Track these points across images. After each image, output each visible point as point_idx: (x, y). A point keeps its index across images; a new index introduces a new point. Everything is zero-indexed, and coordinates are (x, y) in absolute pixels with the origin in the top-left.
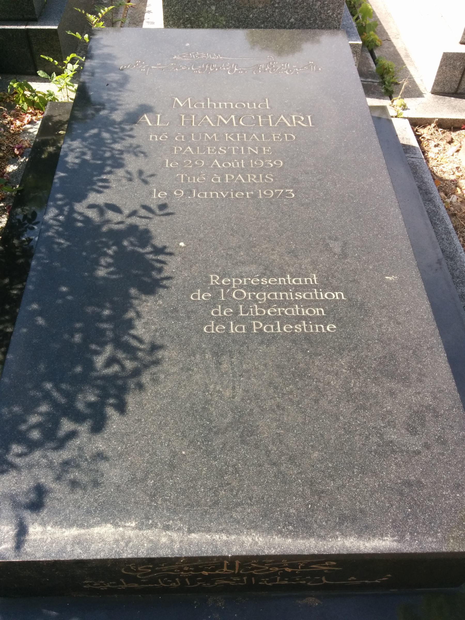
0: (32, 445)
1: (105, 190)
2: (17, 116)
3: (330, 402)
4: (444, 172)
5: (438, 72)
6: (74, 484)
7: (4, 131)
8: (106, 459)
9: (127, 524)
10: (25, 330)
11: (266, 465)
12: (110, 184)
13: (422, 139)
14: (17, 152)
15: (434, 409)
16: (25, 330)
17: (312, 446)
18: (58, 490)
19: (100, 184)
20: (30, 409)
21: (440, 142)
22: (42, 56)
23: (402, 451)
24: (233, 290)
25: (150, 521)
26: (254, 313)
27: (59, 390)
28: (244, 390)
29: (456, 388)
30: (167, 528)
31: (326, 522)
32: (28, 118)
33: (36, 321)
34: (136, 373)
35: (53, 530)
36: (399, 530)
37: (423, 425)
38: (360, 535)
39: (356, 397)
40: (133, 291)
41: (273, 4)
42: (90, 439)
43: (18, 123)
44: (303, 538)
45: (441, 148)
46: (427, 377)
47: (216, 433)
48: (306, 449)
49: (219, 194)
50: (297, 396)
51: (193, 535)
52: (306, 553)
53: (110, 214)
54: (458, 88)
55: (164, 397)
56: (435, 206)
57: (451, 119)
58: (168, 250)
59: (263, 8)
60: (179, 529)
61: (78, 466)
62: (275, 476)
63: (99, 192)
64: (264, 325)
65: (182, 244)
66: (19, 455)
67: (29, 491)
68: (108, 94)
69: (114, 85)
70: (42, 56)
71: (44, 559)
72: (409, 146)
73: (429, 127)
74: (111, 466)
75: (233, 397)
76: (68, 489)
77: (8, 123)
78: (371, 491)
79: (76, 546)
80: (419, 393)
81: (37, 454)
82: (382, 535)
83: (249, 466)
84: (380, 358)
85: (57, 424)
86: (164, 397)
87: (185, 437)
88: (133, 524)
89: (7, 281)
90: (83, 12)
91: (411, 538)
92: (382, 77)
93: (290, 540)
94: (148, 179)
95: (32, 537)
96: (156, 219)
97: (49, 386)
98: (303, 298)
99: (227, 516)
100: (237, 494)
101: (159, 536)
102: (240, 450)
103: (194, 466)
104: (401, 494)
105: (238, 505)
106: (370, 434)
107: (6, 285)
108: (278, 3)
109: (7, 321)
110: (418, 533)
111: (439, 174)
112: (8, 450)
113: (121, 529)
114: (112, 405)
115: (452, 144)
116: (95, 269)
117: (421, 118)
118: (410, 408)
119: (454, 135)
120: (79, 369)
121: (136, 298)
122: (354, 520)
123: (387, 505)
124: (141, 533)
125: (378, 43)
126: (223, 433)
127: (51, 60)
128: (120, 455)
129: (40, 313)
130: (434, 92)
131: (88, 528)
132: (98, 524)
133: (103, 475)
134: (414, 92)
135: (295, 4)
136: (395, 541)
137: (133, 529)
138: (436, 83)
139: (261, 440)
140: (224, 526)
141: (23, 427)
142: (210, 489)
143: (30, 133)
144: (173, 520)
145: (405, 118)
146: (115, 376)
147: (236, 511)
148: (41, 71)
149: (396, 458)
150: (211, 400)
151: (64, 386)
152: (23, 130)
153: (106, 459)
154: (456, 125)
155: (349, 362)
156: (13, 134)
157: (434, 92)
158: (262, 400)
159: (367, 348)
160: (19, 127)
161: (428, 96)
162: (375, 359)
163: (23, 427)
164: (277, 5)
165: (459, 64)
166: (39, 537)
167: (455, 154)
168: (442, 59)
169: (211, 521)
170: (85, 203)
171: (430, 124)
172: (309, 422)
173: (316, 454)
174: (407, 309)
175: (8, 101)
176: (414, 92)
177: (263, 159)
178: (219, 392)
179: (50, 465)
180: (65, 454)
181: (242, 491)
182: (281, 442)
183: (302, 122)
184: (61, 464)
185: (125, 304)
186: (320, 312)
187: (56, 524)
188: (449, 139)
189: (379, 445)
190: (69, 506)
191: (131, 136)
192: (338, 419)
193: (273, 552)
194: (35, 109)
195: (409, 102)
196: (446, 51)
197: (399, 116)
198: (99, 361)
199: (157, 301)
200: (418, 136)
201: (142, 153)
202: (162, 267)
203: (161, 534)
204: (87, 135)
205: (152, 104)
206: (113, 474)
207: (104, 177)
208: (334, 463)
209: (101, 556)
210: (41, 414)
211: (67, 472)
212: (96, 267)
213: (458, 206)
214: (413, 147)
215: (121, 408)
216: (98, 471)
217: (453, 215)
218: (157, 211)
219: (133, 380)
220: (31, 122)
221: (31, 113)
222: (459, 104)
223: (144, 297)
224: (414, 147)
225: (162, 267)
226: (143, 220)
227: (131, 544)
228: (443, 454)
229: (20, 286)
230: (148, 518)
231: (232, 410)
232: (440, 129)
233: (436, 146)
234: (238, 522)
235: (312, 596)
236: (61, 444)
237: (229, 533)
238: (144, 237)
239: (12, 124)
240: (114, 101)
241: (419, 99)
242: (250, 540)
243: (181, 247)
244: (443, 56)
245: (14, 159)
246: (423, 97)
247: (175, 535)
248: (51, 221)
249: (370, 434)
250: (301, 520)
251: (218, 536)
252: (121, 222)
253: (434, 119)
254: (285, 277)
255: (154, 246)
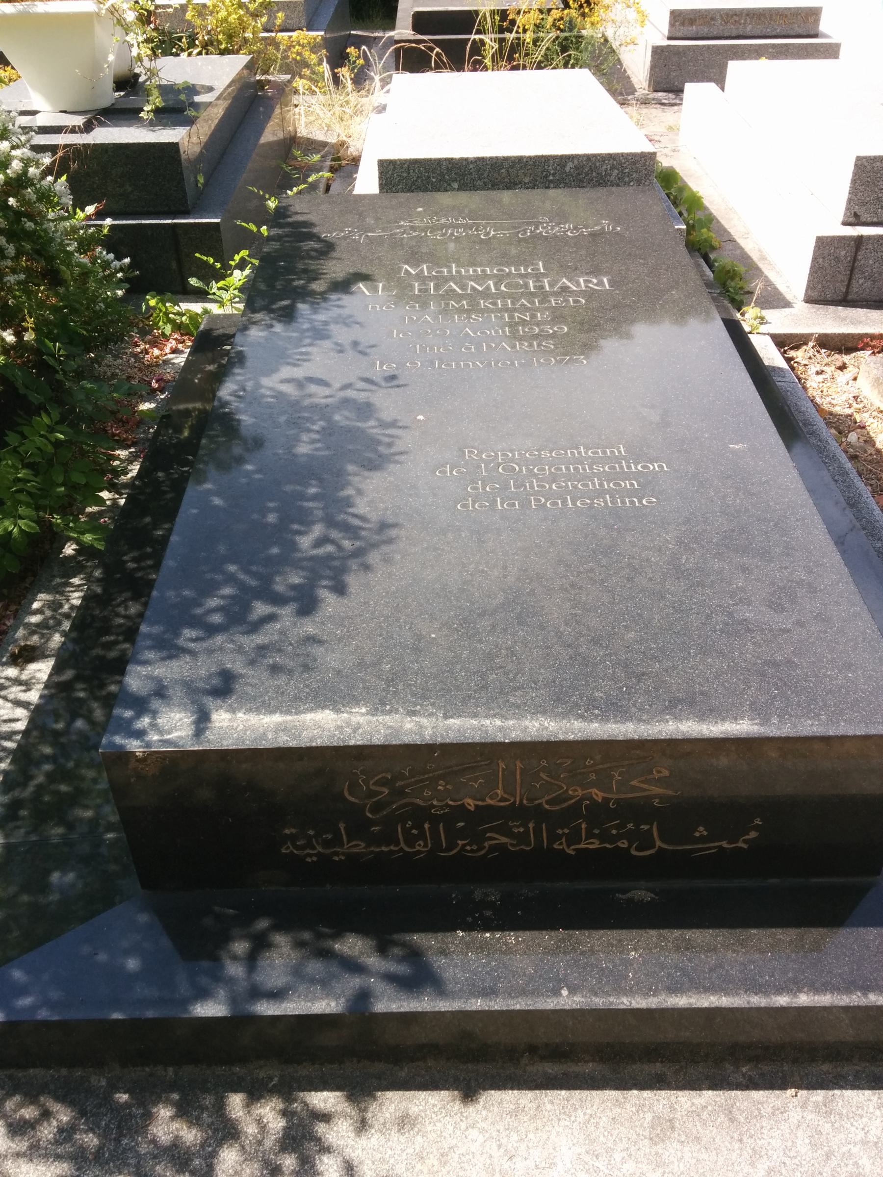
0: (212, 630)
1: (305, 363)
2: (154, 343)
3: (650, 579)
4: (834, 406)
5: (811, 268)
6: (275, 669)
7: (135, 362)
8: (320, 642)
9: (354, 710)
10: (195, 511)
11: (557, 647)
12: (312, 357)
13: (795, 365)
14: (155, 385)
15: (810, 585)
16: (195, 511)
17: (625, 627)
18: (252, 677)
19: (298, 357)
20: (209, 589)
21: (826, 369)
22: (197, 255)
23: (762, 630)
24: (499, 465)
25: (388, 707)
26: (532, 487)
27: (248, 572)
28: (521, 570)
29: (842, 561)
30: (413, 713)
31: (650, 706)
32: (172, 344)
33: (211, 501)
34: (358, 553)
35: (246, 717)
36: (759, 712)
37: (793, 601)
38: (701, 718)
39: (690, 574)
40: (351, 468)
41: (546, 177)
42: (295, 623)
43: (156, 352)
44: (616, 722)
45: (827, 376)
46: (797, 550)
47: (479, 615)
48: (616, 630)
49: (473, 364)
50: (600, 574)
51: (451, 721)
52: (621, 738)
53: (313, 388)
54: (847, 293)
55: (402, 578)
56: (820, 440)
57: (839, 334)
58: (400, 424)
59: (530, 182)
60: (431, 715)
61: (279, 650)
62: (571, 658)
63: (295, 365)
64: (546, 501)
65: (421, 417)
66: (192, 640)
67: (210, 676)
68: (306, 264)
69: (313, 254)
70: (197, 255)
71: (234, 747)
72: (773, 367)
73: (805, 347)
74: (327, 650)
75: (505, 577)
76: (266, 674)
77: (142, 352)
78: (716, 672)
79: (281, 734)
80: (786, 568)
81: (219, 639)
82: (736, 719)
83: (530, 649)
84: (725, 532)
85: (247, 608)
86: (402, 578)
87: (435, 619)
88: (364, 710)
89: (148, 519)
90: (261, 193)
91: (780, 721)
92: (724, 285)
93: (597, 725)
94: (368, 350)
95: (217, 725)
96: (381, 393)
97: (232, 568)
98: (604, 471)
99: (500, 700)
100: (514, 678)
101: (402, 722)
102: (518, 631)
103: (449, 649)
104: (763, 675)
105: (516, 689)
106: (712, 613)
107: (148, 524)
108: (554, 175)
109: (150, 567)
110: (790, 716)
111: (826, 407)
112: (177, 635)
113: (345, 715)
114: (325, 587)
115: (845, 371)
116: (295, 446)
117: (791, 334)
118: (773, 583)
119: (846, 358)
120: (275, 550)
121: (356, 475)
122: (692, 703)
123: (742, 687)
124: (375, 718)
125: (715, 243)
126: (491, 615)
127: (211, 260)
128: (340, 640)
129: (218, 494)
130: (809, 300)
131: (296, 714)
132: (312, 710)
133: (316, 660)
134: (774, 300)
135: (579, 174)
136: (756, 724)
137: (363, 715)
138: (810, 286)
139: (548, 622)
140: (497, 711)
141: (199, 611)
142: (475, 673)
143: (174, 364)
144: (421, 705)
145: (764, 334)
146: (330, 557)
147: (515, 696)
148: (194, 279)
149: (753, 637)
150: (472, 580)
151: (254, 568)
152: (164, 361)
153: (320, 642)
154: (850, 345)
155: (678, 537)
156: (148, 366)
157: (809, 300)
158: (547, 580)
159: (705, 522)
160: (157, 357)
161: (800, 307)
162: (717, 533)
163: (199, 611)
164: (551, 178)
165: (843, 253)
166: (225, 724)
167: (851, 382)
168: (815, 247)
169: (477, 706)
170: (276, 377)
171: (806, 344)
172: (620, 601)
173: (632, 635)
174: (764, 479)
175: (141, 326)
176: (774, 300)
177: (538, 325)
178: (483, 571)
179: (240, 650)
180: (260, 639)
181: (523, 675)
182: (577, 623)
183: (596, 285)
184: (254, 649)
185: (339, 478)
186: (632, 485)
187: (250, 710)
188: (839, 364)
189: (727, 624)
190: (268, 692)
191: (339, 306)
192: (663, 598)
193: (571, 737)
194: (182, 335)
195: (768, 314)
196: (820, 235)
197: (755, 332)
198: (305, 542)
199: (386, 478)
200: (789, 360)
201: (358, 323)
202: (392, 442)
203: (405, 721)
204: (274, 307)
205: (370, 272)
206: (331, 659)
207: (304, 350)
208: (659, 644)
209: (319, 743)
210: (223, 597)
211: (264, 657)
212: (295, 443)
213: (861, 447)
214: (779, 368)
215: (340, 589)
216: (308, 656)
217: (853, 458)
218: (383, 384)
219: (356, 560)
220: (174, 351)
221: (176, 339)
222: (851, 314)
223: (366, 473)
224: (781, 369)
225: (392, 442)
226: (362, 393)
227: (361, 731)
228: (825, 632)
229: (167, 526)
230: (384, 704)
231: (503, 590)
232: (824, 351)
233: (818, 373)
234: (518, 707)
235: (640, 889)
236: (255, 627)
237: (503, 717)
238: (365, 410)
239: (147, 353)
240: (313, 271)
241: (787, 310)
242: (537, 725)
243: (419, 420)
244: (817, 242)
245: (151, 395)
246: (792, 307)
247: (425, 721)
248: (228, 398)
249: (712, 613)
250: (613, 704)
251: (488, 722)
252: (331, 396)
253: (812, 335)
254: (577, 448)
255: (378, 420)
